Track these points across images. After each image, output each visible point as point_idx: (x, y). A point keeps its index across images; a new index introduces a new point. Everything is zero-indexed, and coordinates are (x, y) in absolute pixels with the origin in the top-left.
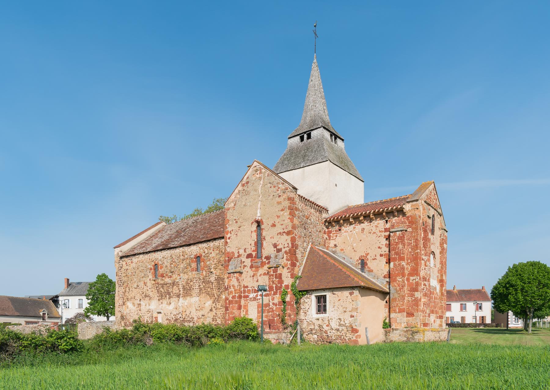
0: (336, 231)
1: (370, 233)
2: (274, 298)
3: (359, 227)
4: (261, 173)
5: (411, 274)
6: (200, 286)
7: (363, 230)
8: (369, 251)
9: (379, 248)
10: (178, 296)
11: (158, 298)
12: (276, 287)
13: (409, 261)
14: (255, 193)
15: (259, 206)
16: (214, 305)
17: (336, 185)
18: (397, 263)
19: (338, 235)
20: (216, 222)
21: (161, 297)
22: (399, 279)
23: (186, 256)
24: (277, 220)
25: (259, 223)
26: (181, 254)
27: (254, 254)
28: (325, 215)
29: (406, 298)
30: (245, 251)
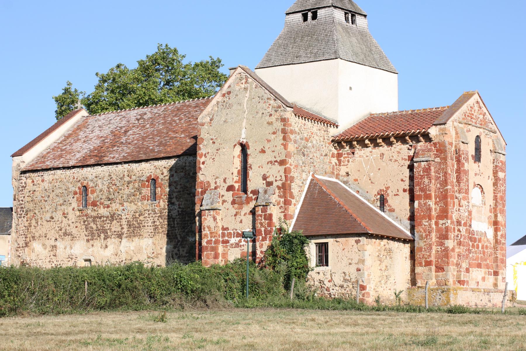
0: (348, 154)
1: (391, 160)
2: (262, 245)
3: (378, 151)
4: (246, 82)
5: (439, 217)
6: (154, 222)
7: (382, 155)
8: (390, 185)
9: (402, 180)
10: (120, 236)
11: (86, 238)
12: (265, 230)
13: (438, 200)
14: (239, 107)
15: (244, 124)
16: (176, 251)
17: (351, 88)
18: (422, 201)
19: (351, 160)
20: (177, 124)
21: (92, 236)
22: (425, 222)
23: (134, 178)
24: (267, 145)
25: (244, 148)
26: (126, 173)
27: (237, 186)
28: (333, 132)
29: (434, 248)
30: (225, 181)
